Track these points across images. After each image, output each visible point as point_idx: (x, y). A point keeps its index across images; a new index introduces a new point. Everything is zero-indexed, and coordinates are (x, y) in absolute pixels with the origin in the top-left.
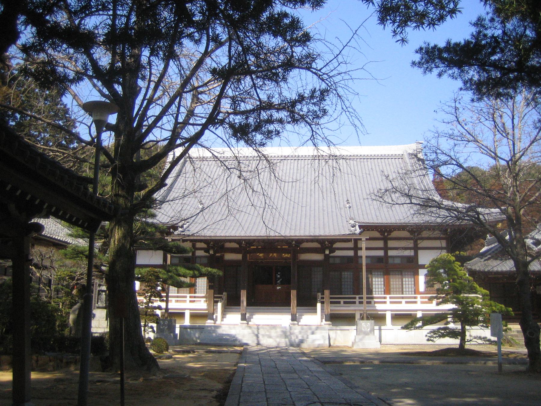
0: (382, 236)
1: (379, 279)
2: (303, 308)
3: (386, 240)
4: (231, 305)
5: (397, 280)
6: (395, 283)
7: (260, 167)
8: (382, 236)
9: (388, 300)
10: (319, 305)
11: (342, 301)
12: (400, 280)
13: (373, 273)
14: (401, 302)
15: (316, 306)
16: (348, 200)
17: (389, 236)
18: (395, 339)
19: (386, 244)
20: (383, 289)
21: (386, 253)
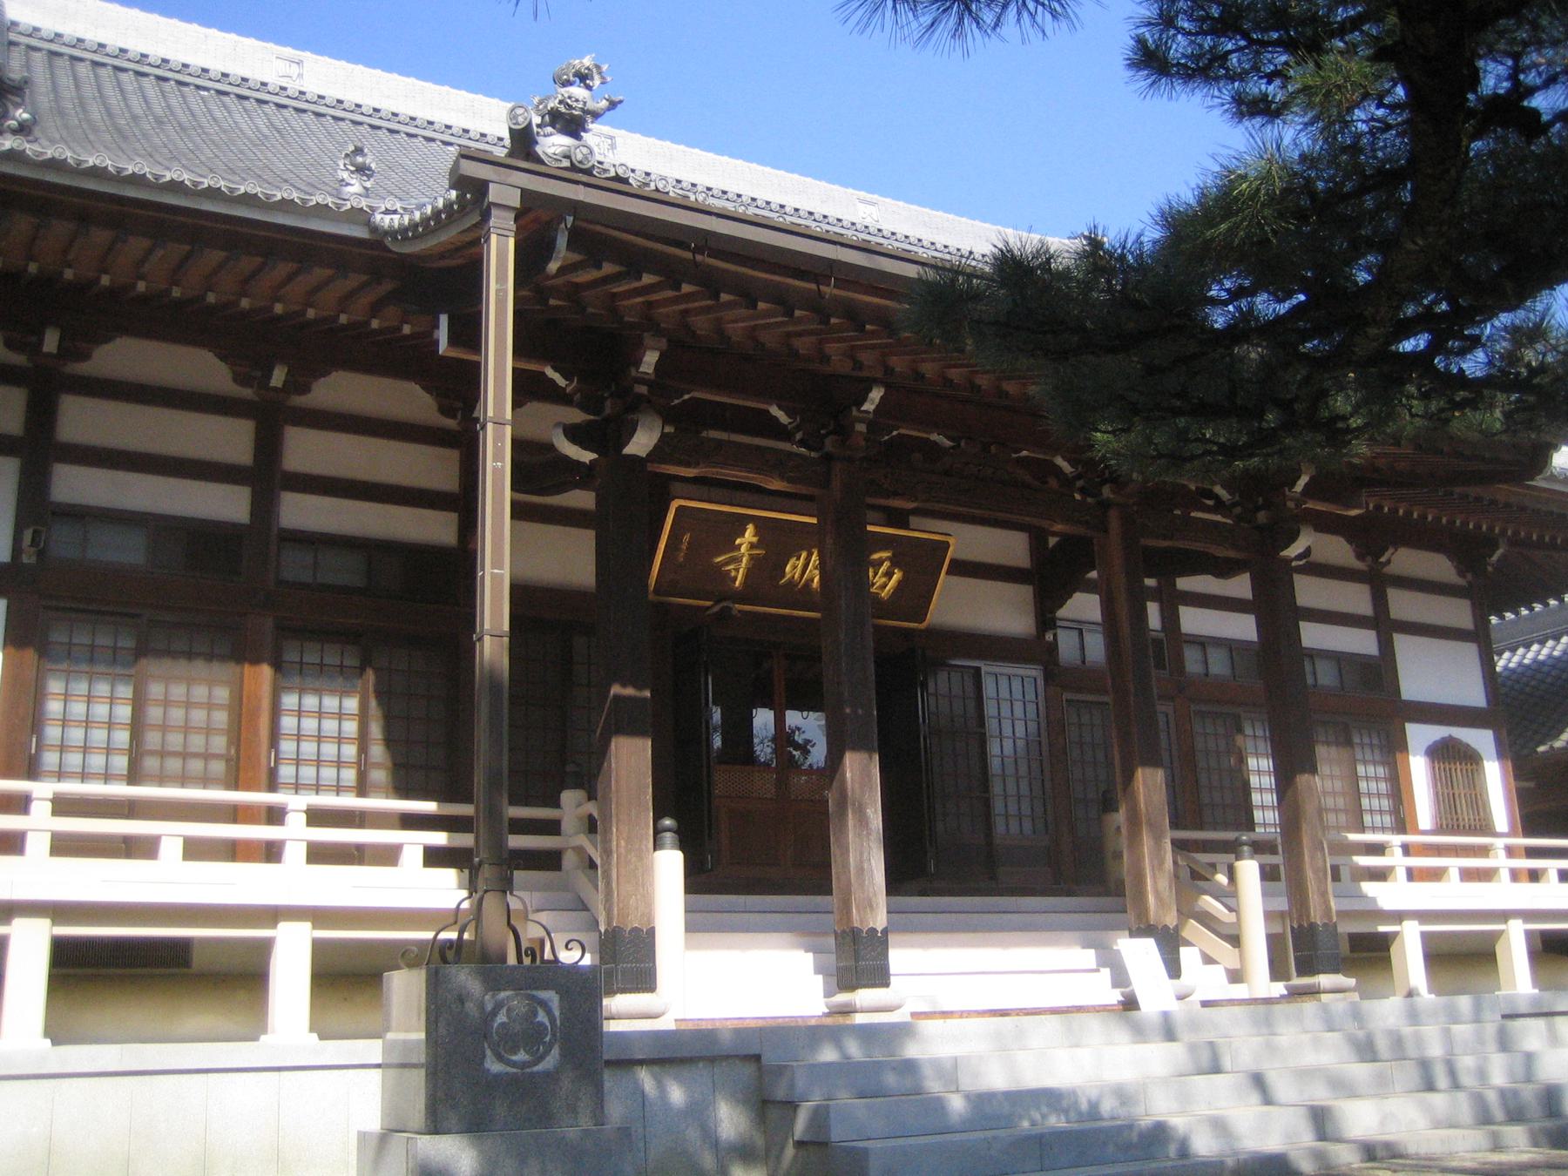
3: (271, 420)
4: (826, 867)
6: (78, 709)
7: (1363, 117)
14: (388, 856)
17: (299, 401)
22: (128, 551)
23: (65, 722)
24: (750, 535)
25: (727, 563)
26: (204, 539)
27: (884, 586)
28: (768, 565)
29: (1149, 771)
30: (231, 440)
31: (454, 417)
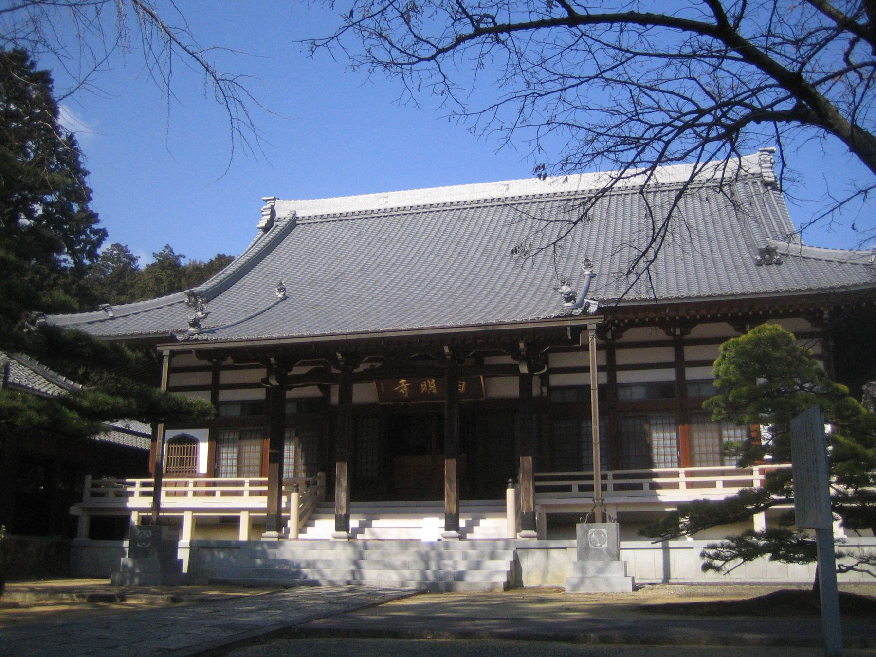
0: (670, 338)
1: (667, 434)
2: (371, 503)
3: (679, 345)
5: (709, 434)
6: (703, 441)
8: (670, 338)
9: (682, 479)
10: (510, 493)
11: (575, 484)
12: (716, 434)
13: (653, 422)
15: (503, 497)
16: (587, 260)
18: (684, 568)
19: (679, 354)
20: (676, 457)
21: (681, 374)
22: (235, 412)
23: (658, 447)
26: (664, 389)
29: (449, 461)
30: (667, 354)
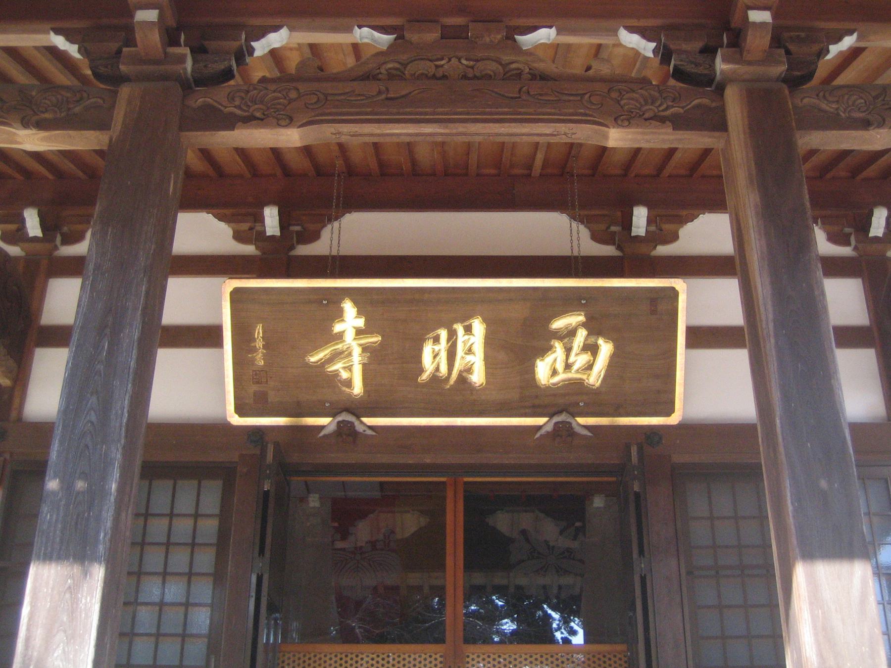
24: (350, 320)
25: (331, 359)
27: (589, 367)
28: (393, 359)
31: (847, 243)
